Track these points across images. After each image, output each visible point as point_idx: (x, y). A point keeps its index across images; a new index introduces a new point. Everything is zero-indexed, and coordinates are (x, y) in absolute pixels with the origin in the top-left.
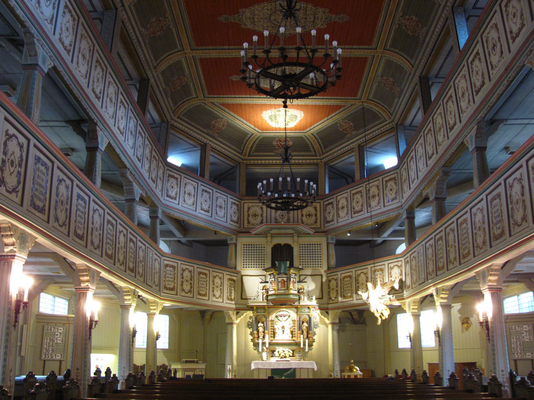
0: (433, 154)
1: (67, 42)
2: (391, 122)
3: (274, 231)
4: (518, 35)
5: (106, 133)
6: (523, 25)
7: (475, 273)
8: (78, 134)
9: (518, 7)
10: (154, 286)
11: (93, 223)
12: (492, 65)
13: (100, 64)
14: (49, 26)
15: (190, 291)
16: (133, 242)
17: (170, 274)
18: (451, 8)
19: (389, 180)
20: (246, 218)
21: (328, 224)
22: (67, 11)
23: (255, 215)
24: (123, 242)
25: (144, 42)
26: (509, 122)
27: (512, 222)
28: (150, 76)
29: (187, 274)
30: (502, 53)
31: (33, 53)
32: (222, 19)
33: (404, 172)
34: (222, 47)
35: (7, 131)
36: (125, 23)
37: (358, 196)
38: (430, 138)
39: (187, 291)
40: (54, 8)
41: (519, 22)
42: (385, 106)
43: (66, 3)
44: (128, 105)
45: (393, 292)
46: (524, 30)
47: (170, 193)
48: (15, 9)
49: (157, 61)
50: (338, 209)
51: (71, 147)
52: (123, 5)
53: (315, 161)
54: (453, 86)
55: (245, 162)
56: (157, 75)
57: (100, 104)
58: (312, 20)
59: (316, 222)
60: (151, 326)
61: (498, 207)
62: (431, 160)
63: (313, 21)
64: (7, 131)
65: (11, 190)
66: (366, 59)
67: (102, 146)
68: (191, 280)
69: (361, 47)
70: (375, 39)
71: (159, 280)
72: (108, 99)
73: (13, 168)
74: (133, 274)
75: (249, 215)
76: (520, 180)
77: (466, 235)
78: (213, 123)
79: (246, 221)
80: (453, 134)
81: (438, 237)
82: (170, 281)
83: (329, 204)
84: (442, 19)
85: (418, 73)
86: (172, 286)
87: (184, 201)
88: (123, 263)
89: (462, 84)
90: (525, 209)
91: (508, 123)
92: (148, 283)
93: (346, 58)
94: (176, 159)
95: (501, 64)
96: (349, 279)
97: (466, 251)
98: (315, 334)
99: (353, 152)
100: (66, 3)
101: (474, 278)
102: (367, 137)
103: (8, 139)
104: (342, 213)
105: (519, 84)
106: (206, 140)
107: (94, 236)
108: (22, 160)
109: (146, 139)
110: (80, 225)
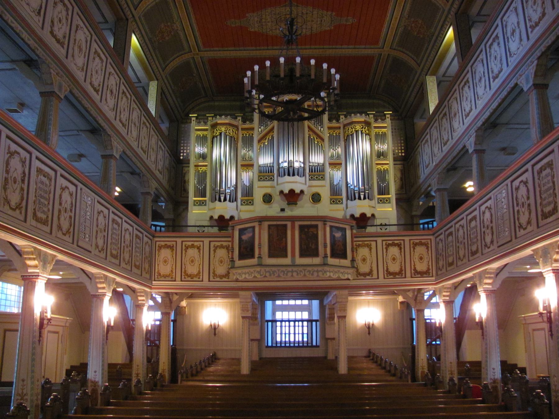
4: (537, 24)
6: (544, 14)
7: (533, 250)
10: (95, 252)
11: (60, 204)
14: (36, 18)
16: (117, 223)
41: (540, 10)
44: (150, 125)
54: (484, 50)
61: (550, 178)
72: (109, 92)
74: (117, 262)
77: (475, 230)
88: (103, 249)
92: (80, 244)
101: (531, 257)
108: (24, 176)
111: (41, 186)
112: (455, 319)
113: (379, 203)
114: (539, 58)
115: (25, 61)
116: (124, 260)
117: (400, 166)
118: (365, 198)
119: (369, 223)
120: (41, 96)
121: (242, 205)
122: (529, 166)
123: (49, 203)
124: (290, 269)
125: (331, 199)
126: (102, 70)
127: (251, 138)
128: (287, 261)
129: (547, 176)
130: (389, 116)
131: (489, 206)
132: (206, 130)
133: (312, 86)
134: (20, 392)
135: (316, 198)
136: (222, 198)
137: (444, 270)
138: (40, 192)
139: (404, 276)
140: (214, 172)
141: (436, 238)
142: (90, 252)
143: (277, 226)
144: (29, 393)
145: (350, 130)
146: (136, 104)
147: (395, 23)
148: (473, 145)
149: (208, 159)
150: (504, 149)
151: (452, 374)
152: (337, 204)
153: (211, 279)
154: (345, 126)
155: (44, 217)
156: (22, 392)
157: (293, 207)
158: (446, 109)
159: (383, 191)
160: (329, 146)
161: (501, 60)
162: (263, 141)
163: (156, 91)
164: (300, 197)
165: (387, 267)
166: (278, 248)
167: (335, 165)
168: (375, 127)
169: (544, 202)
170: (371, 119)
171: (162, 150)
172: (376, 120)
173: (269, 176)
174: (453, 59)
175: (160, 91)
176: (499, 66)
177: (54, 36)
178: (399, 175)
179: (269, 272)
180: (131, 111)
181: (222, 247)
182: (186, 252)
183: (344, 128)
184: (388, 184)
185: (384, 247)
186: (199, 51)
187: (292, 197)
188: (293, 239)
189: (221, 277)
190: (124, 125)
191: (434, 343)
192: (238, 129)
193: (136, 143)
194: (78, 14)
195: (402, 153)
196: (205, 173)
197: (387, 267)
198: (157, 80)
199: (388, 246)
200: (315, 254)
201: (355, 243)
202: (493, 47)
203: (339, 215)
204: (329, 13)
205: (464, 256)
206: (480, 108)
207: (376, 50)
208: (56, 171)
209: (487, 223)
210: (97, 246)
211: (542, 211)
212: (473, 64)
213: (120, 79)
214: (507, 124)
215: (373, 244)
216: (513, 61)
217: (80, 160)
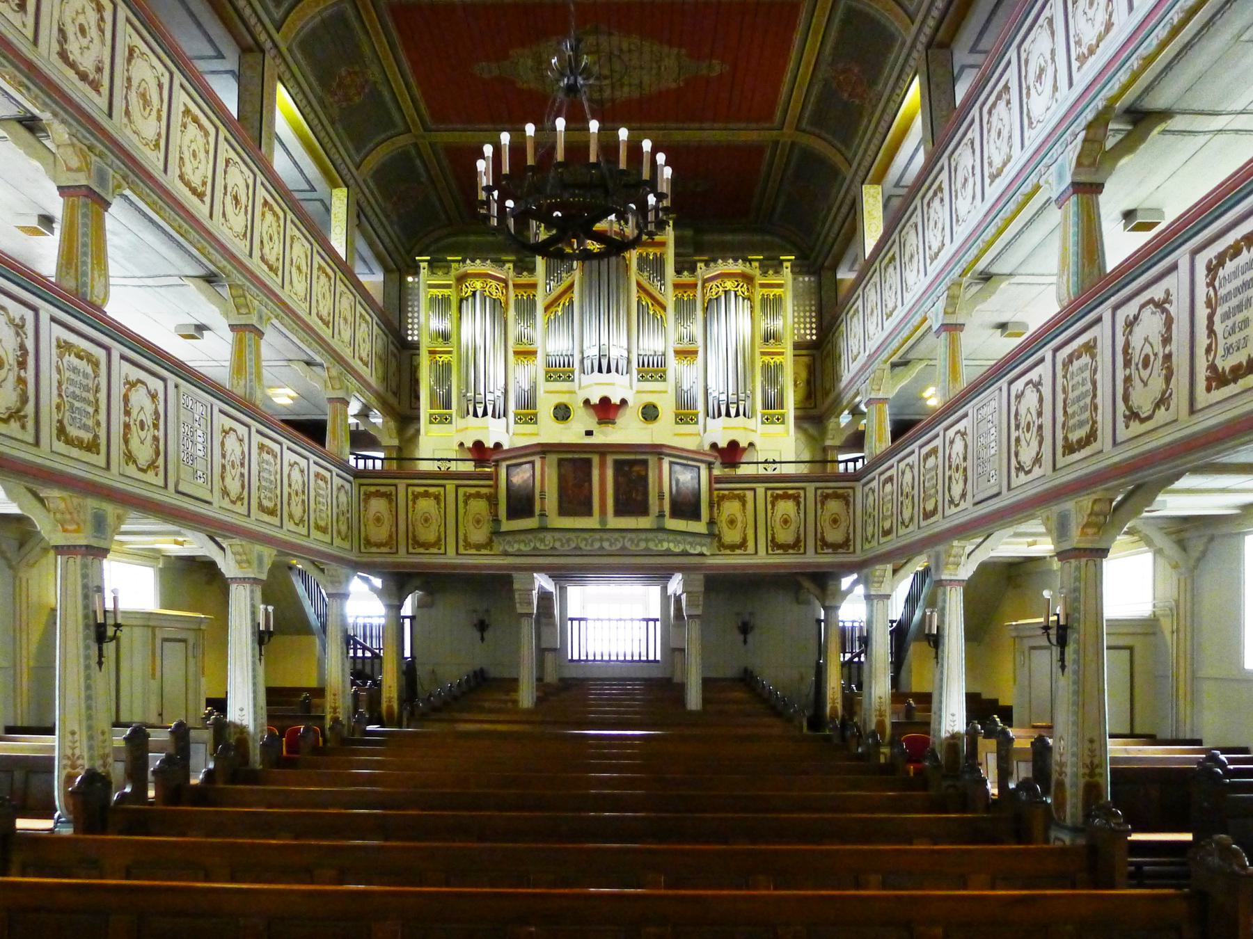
4: (1092, 51)
6: (1109, 26)
11: (290, 485)
13: (271, 209)
26: (1177, 123)
27: (1014, 462)
30: (1055, 88)
41: (1101, 17)
54: (946, 168)
57: (279, 281)
61: (1087, 374)
72: (229, 199)
76: (1037, 385)
111: (73, 376)
112: (892, 622)
113: (763, 423)
114: (1089, 126)
115: (20, 121)
116: (291, 516)
117: (805, 359)
118: (737, 414)
119: (745, 458)
120: (61, 195)
121: (516, 423)
122: (1047, 352)
123: (96, 411)
124: (597, 536)
125: (677, 415)
126: (207, 152)
127: (532, 304)
128: (591, 522)
129: (1081, 370)
130: (788, 264)
131: (963, 430)
132: (448, 286)
133: (619, 185)
134: (69, 752)
135: (650, 413)
136: (480, 411)
138: (71, 389)
139: (802, 550)
140: (463, 364)
141: (864, 485)
142: (209, 503)
143: (573, 461)
144: (86, 755)
145: (715, 289)
146: (299, 229)
147: (805, 73)
148: (941, 315)
149: (454, 339)
150: (1003, 326)
151: (881, 715)
152: (688, 423)
153: (461, 550)
154: (705, 281)
155: (86, 436)
156: (73, 755)
157: (610, 428)
158: (896, 248)
159: (773, 403)
160: (676, 320)
161: (1010, 137)
162: (553, 309)
163: (345, 208)
164: (621, 411)
165: (773, 535)
166: (575, 499)
167: (685, 354)
168: (762, 286)
169: (1071, 422)
170: (754, 270)
171: (367, 322)
172: (765, 273)
173: (564, 373)
174: (917, 150)
175: (354, 209)
176: (1005, 149)
178: (804, 375)
179: (560, 540)
181: (478, 495)
182: (414, 503)
183: (703, 287)
184: (782, 388)
185: (769, 499)
186: (425, 130)
187: (606, 410)
188: (603, 481)
189: (478, 547)
191: (856, 659)
192: (507, 286)
193: (306, 306)
195: (812, 334)
196: (447, 367)
197: (773, 535)
198: (347, 186)
199: (776, 498)
200: (643, 510)
201: (716, 493)
203: (690, 444)
204: (675, 51)
205: (911, 519)
206: (959, 239)
207: (767, 133)
208: (108, 350)
209: (956, 460)
210: (225, 492)
211: (1066, 439)
212: (953, 152)
213: (255, 176)
214: (1011, 275)
215: (750, 494)
216: (1035, 137)
217: (202, 336)
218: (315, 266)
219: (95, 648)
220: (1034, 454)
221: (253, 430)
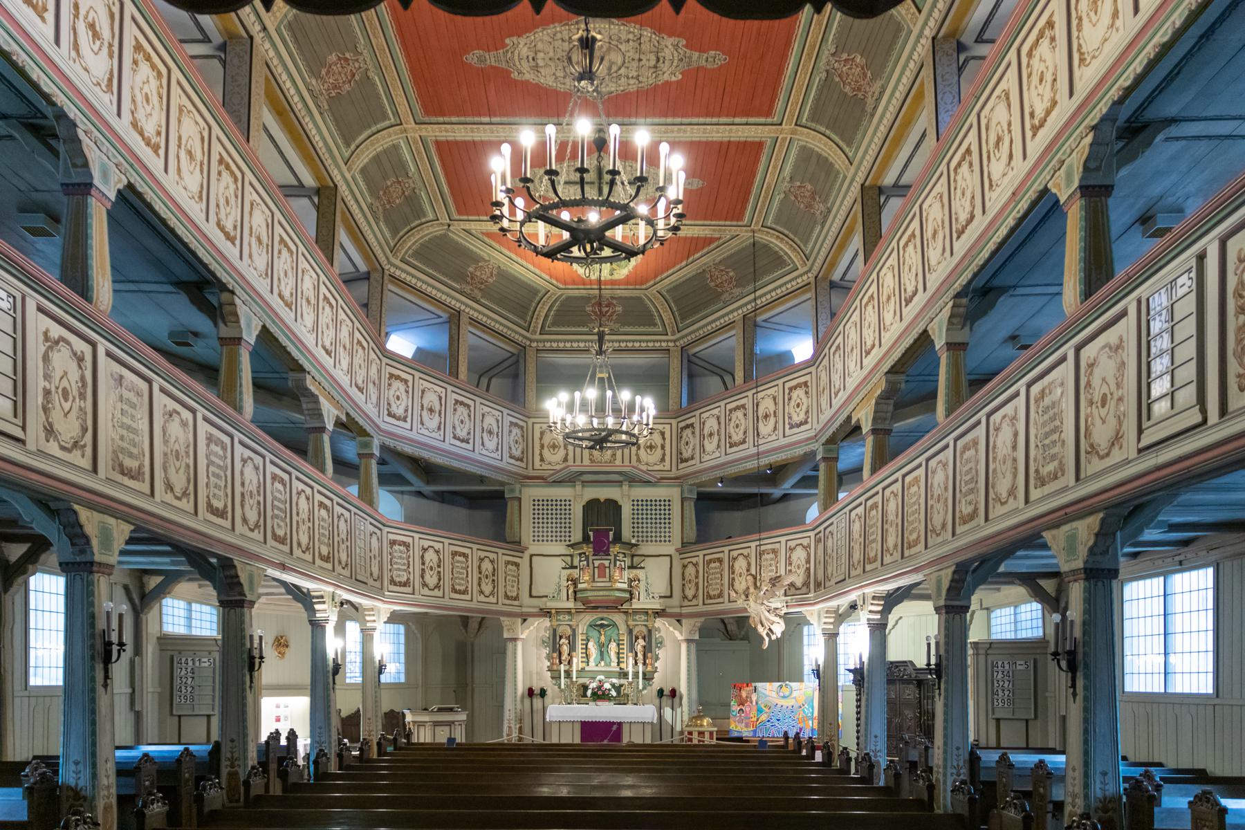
0: (873, 346)
1: (150, 128)
2: (806, 273)
3: (585, 477)
5: (256, 308)
6: (1054, 103)
8: (201, 309)
9: (1050, 63)
10: (371, 582)
11: (243, 484)
12: (990, 180)
13: (228, 167)
14: (106, 98)
15: (437, 587)
16: (326, 507)
17: (400, 558)
18: (930, 40)
19: (795, 387)
20: (537, 452)
21: (684, 465)
22: (140, 57)
23: (554, 447)
24: (306, 510)
25: (318, 107)
27: (992, 495)
28: (338, 178)
29: (430, 556)
30: (1011, 156)
31: (79, 162)
32: (472, 58)
33: (890, 275)
34: (476, 119)
35: (46, 333)
36: (274, 70)
37: (740, 414)
38: (871, 315)
39: (431, 586)
40: (111, 56)
41: (1048, 95)
42: (796, 239)
43: (136, 38)
45: (793, 591)
46: (1054, 114)
47: (394, 409)
48: (27, 69)
49: (348, 146)
50: (702, 437)
51: (193, 329)
52: (264, 29)
53: (664, 344)
55: (534, 345)
56: (353, 178)
57: (236, 251)
58: (653, 63)
59: (663, 460)
60: (372, 644)
62: (870, 357)
63: (655, 67)
64: (46, 333)
65: (69, 446)
66: (760, 145)
67: (250, 334)
68: (439, 566)
69: (751, 120)
70: (779, 104)
71: (381, 569)
72: (253, 240)
73: (69, 403)
75: (542, 446)
78: (471, 269)
79: (537, 458)
80: (910, 312)
81: (870, 503)
82: (399, 570)
83: (687, 427)
84: (912, 64)
85: (860, 178)
86: (404, 579)
87: (422, 424)
88: (308, 549)
89: (998, 115)
90: (1015, 476)
91: (1016, 293)
93: (722, 143)
94: (402, 344)
95: (1006, 180)
96: (717, 564)
97: (914, 536)
98: (657, 659)
99: (733, 328)
100: (136, 38)
102: (758, 302)
103: (51, 348)
104: (710, 446)
105: (1041, 221)
106: (458, 305)
107: (247, 507)
108: (84, 385)
109: (340, 310)
110: (216, 491)
137: (897, 555)
171: (363, 348)
177: (222, 229)
180: (298, 274)
190: (328, 353)
194: (133, 19)
202: (1036, 53)
208: (290, 474)
211: (1037, 471)
218: (215, 158)
219: (99, 668)
220: (1009, 486)
221: (236, 441)
